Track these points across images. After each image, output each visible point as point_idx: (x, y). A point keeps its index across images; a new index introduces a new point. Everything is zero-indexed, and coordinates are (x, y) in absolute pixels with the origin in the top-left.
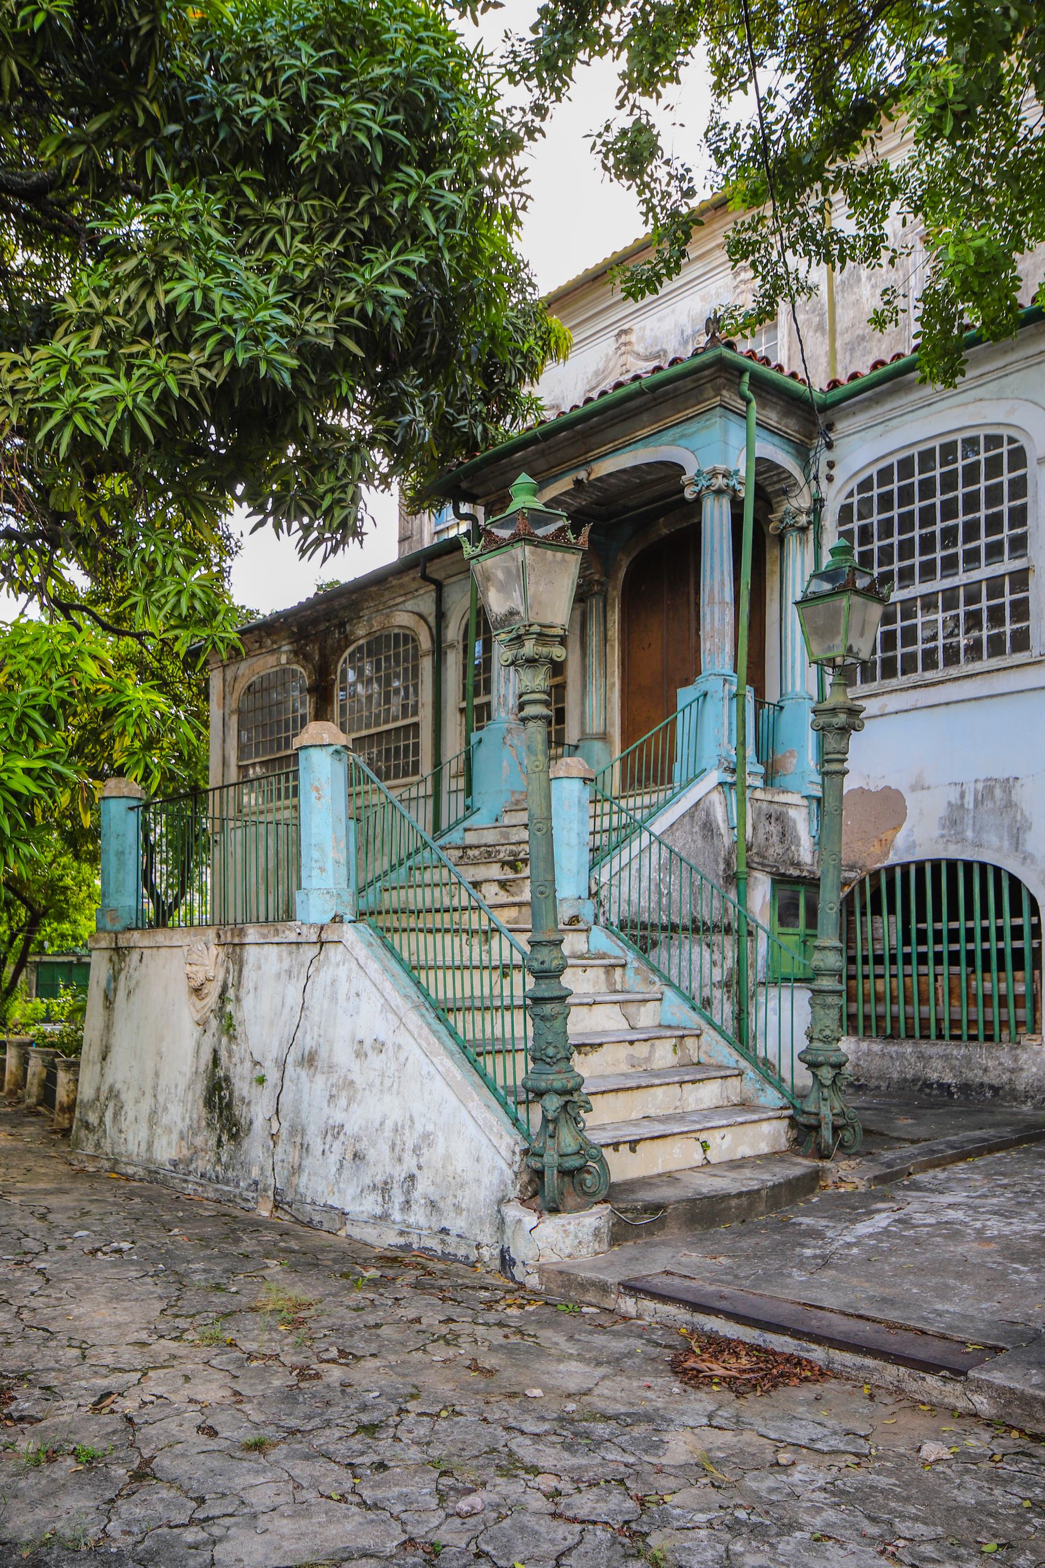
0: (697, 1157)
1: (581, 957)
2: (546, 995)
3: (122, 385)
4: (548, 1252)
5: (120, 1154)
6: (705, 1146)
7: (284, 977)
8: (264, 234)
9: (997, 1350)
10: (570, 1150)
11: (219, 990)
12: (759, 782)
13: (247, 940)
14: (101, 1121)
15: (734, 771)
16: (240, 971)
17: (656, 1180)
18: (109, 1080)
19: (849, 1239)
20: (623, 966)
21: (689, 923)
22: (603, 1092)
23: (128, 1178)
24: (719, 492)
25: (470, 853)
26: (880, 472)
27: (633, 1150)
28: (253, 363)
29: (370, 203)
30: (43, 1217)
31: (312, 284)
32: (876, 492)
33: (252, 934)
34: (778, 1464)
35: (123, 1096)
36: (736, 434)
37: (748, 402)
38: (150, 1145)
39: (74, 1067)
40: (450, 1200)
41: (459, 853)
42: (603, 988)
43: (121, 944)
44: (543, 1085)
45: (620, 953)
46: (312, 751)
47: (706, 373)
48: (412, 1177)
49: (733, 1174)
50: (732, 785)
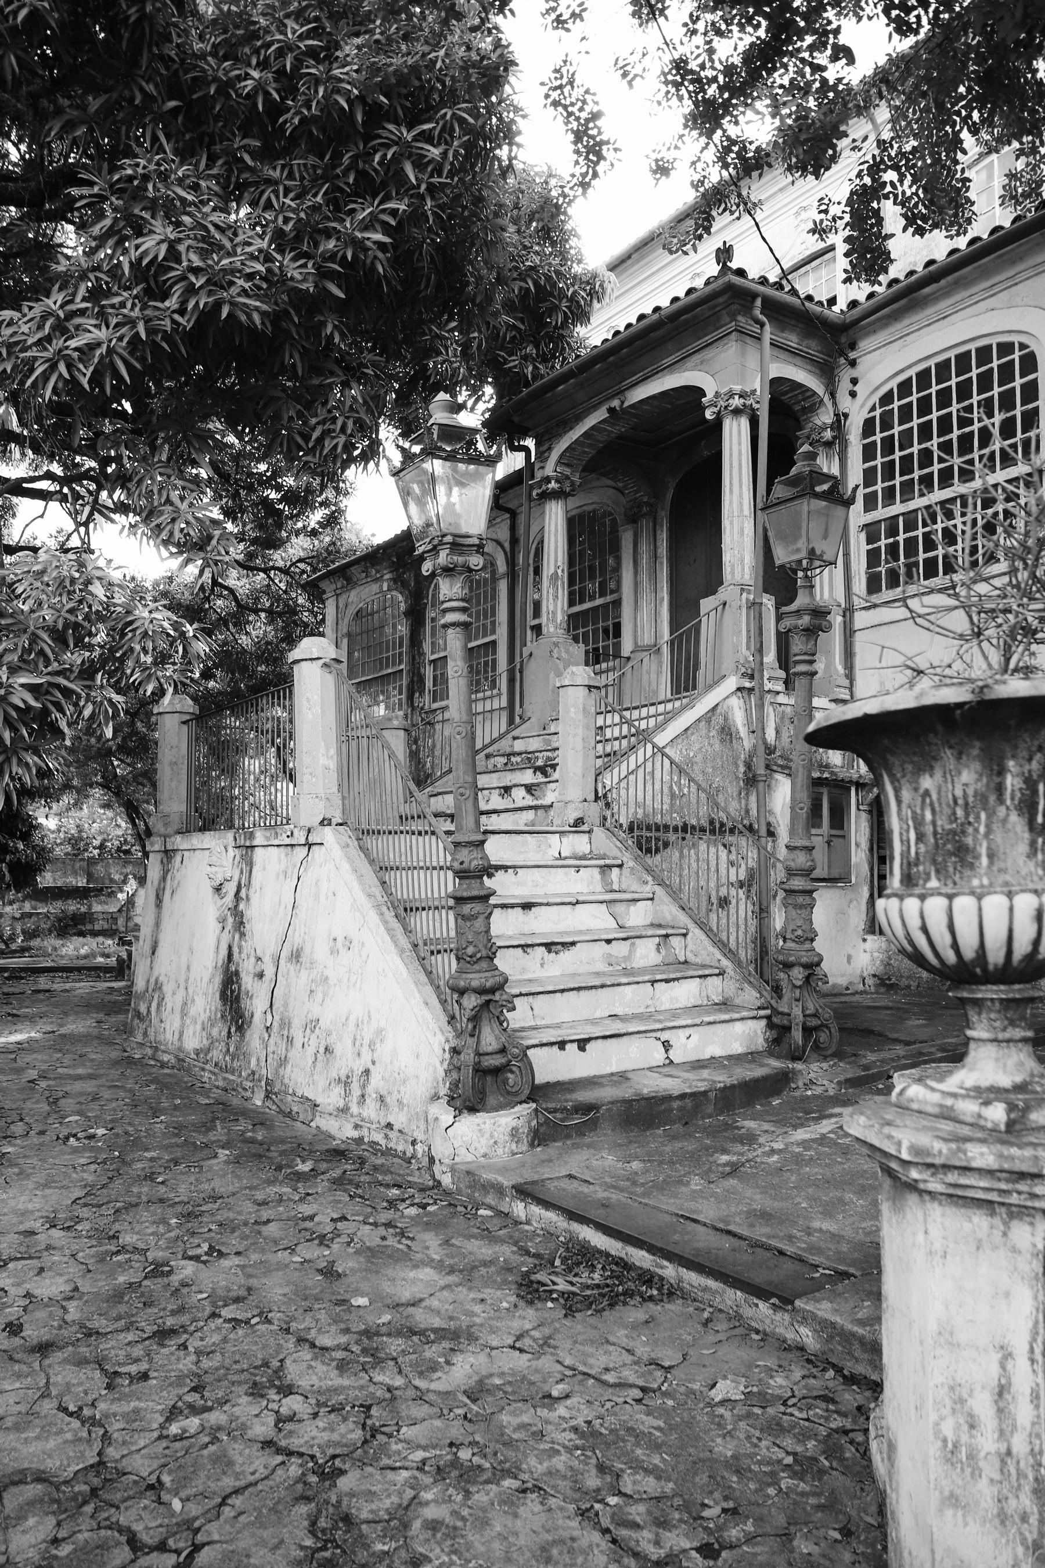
0: (658, 1056)
1: (581, 858)
2: (465, 894)
3: (102, 334)
4: (463, 1151)
5: (160, 1042)
6: (667, 1045)
7: (282, 877)
8: (263, 192)
9: (845, 1275)
10: (490, 1049)
11: (235, 889)
12: (780, 687)
13: (255, 843)
14: (149, 1011)
15: (752, 677)
17: (603, 1080)
18: (156, 973)
19: (776, 1146)
20: (620, 866)
21: (706, 825)
22: (563, 991)
24: (737, 412)
25: (513, 759)
26: (900, 386)
27: (582, 1049)
28: (218, 305)
29: (355, 158)
31: (298, 238)
32: (897, 404)
33: (259, 838)
34: (549, 1396)
35: (165, 988)
36: (752, 360)
37: (762, 325)
38: (181, 1034)
40: (395, 1096)
41: (504, 760)
42: (599, 888)
43: (169, 847)
44: (462, 983)
45: (619, 854)
46: (303, 663)
47: (721, 300)
48: (367, 1072)
49: (686, 1075)
50: (751, 690)
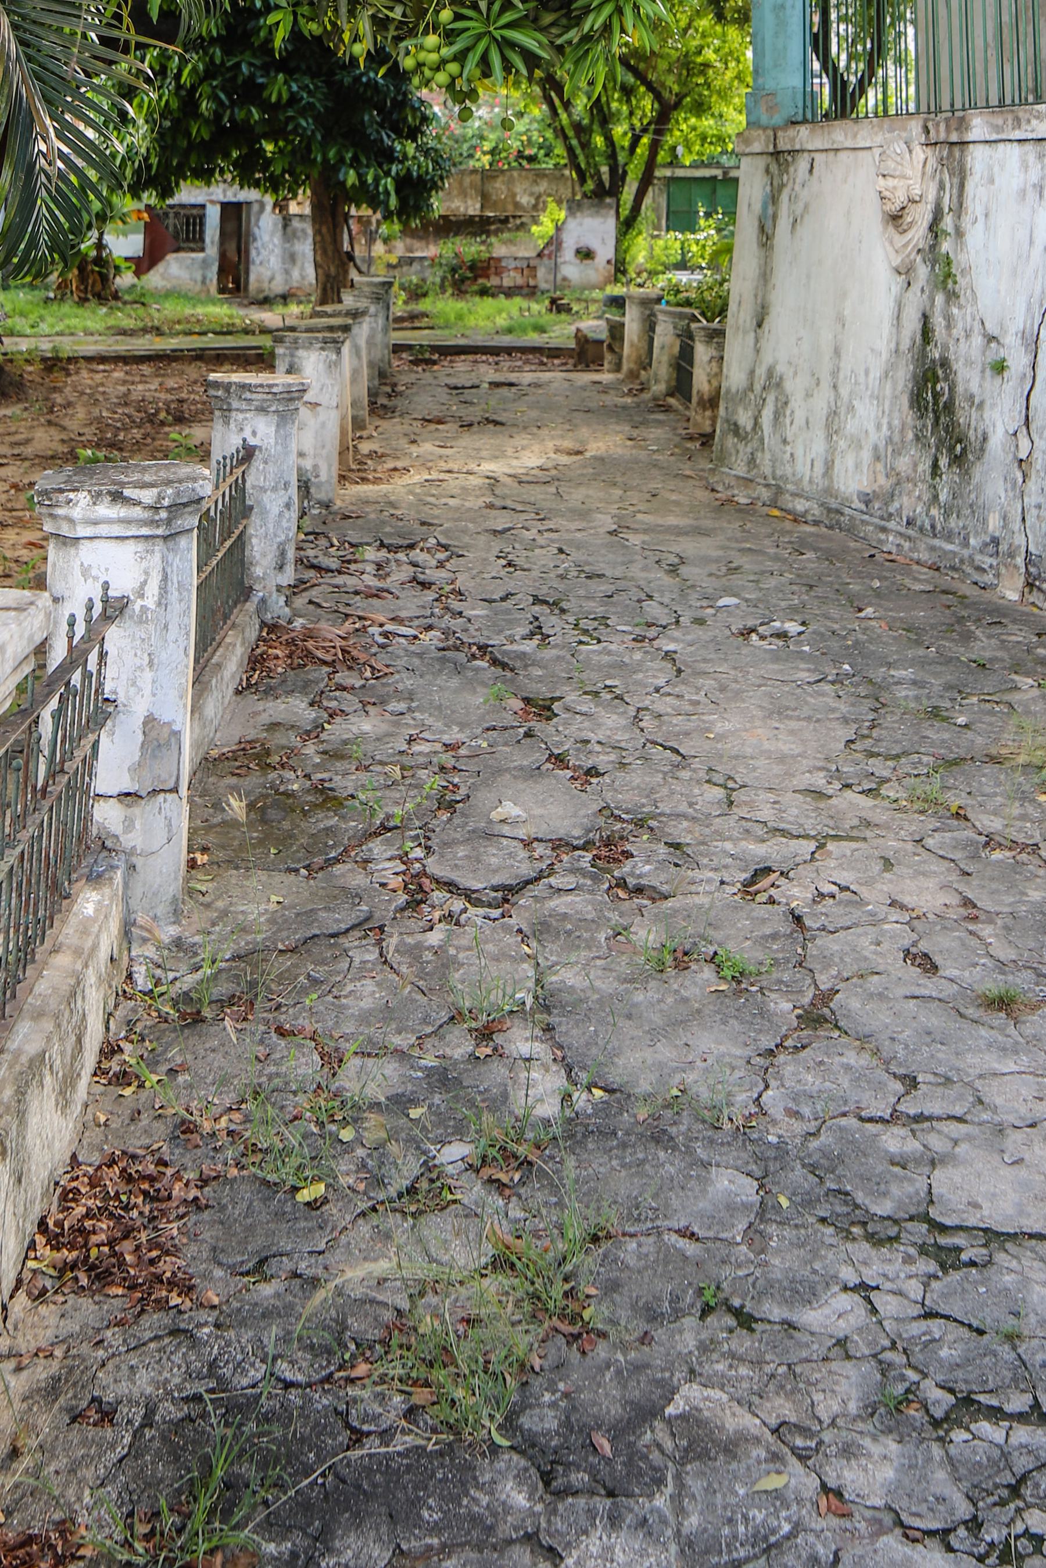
7: (1032, 195)
11: (928, 217)
13: (971, 136)
14: (756, 424)
16: (962, 186)
18: (767, 359)
23: (798, 519)
30: (673, 570)
33: (979, 127)
35: (788, 385)
39: (716, 336)
43: (782, 146)
